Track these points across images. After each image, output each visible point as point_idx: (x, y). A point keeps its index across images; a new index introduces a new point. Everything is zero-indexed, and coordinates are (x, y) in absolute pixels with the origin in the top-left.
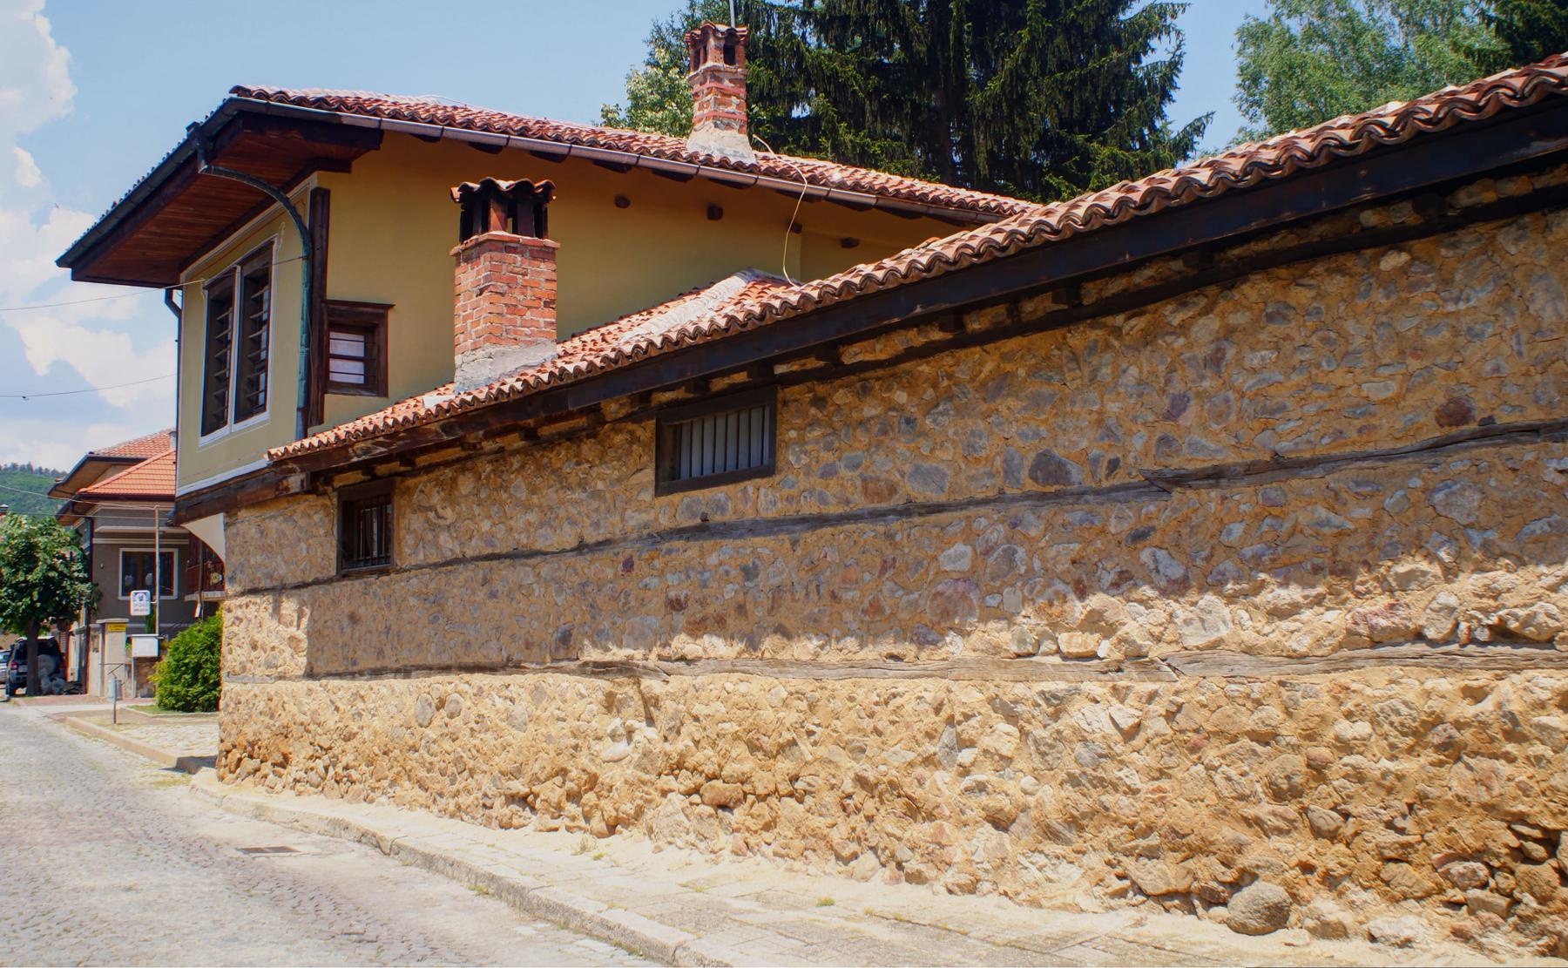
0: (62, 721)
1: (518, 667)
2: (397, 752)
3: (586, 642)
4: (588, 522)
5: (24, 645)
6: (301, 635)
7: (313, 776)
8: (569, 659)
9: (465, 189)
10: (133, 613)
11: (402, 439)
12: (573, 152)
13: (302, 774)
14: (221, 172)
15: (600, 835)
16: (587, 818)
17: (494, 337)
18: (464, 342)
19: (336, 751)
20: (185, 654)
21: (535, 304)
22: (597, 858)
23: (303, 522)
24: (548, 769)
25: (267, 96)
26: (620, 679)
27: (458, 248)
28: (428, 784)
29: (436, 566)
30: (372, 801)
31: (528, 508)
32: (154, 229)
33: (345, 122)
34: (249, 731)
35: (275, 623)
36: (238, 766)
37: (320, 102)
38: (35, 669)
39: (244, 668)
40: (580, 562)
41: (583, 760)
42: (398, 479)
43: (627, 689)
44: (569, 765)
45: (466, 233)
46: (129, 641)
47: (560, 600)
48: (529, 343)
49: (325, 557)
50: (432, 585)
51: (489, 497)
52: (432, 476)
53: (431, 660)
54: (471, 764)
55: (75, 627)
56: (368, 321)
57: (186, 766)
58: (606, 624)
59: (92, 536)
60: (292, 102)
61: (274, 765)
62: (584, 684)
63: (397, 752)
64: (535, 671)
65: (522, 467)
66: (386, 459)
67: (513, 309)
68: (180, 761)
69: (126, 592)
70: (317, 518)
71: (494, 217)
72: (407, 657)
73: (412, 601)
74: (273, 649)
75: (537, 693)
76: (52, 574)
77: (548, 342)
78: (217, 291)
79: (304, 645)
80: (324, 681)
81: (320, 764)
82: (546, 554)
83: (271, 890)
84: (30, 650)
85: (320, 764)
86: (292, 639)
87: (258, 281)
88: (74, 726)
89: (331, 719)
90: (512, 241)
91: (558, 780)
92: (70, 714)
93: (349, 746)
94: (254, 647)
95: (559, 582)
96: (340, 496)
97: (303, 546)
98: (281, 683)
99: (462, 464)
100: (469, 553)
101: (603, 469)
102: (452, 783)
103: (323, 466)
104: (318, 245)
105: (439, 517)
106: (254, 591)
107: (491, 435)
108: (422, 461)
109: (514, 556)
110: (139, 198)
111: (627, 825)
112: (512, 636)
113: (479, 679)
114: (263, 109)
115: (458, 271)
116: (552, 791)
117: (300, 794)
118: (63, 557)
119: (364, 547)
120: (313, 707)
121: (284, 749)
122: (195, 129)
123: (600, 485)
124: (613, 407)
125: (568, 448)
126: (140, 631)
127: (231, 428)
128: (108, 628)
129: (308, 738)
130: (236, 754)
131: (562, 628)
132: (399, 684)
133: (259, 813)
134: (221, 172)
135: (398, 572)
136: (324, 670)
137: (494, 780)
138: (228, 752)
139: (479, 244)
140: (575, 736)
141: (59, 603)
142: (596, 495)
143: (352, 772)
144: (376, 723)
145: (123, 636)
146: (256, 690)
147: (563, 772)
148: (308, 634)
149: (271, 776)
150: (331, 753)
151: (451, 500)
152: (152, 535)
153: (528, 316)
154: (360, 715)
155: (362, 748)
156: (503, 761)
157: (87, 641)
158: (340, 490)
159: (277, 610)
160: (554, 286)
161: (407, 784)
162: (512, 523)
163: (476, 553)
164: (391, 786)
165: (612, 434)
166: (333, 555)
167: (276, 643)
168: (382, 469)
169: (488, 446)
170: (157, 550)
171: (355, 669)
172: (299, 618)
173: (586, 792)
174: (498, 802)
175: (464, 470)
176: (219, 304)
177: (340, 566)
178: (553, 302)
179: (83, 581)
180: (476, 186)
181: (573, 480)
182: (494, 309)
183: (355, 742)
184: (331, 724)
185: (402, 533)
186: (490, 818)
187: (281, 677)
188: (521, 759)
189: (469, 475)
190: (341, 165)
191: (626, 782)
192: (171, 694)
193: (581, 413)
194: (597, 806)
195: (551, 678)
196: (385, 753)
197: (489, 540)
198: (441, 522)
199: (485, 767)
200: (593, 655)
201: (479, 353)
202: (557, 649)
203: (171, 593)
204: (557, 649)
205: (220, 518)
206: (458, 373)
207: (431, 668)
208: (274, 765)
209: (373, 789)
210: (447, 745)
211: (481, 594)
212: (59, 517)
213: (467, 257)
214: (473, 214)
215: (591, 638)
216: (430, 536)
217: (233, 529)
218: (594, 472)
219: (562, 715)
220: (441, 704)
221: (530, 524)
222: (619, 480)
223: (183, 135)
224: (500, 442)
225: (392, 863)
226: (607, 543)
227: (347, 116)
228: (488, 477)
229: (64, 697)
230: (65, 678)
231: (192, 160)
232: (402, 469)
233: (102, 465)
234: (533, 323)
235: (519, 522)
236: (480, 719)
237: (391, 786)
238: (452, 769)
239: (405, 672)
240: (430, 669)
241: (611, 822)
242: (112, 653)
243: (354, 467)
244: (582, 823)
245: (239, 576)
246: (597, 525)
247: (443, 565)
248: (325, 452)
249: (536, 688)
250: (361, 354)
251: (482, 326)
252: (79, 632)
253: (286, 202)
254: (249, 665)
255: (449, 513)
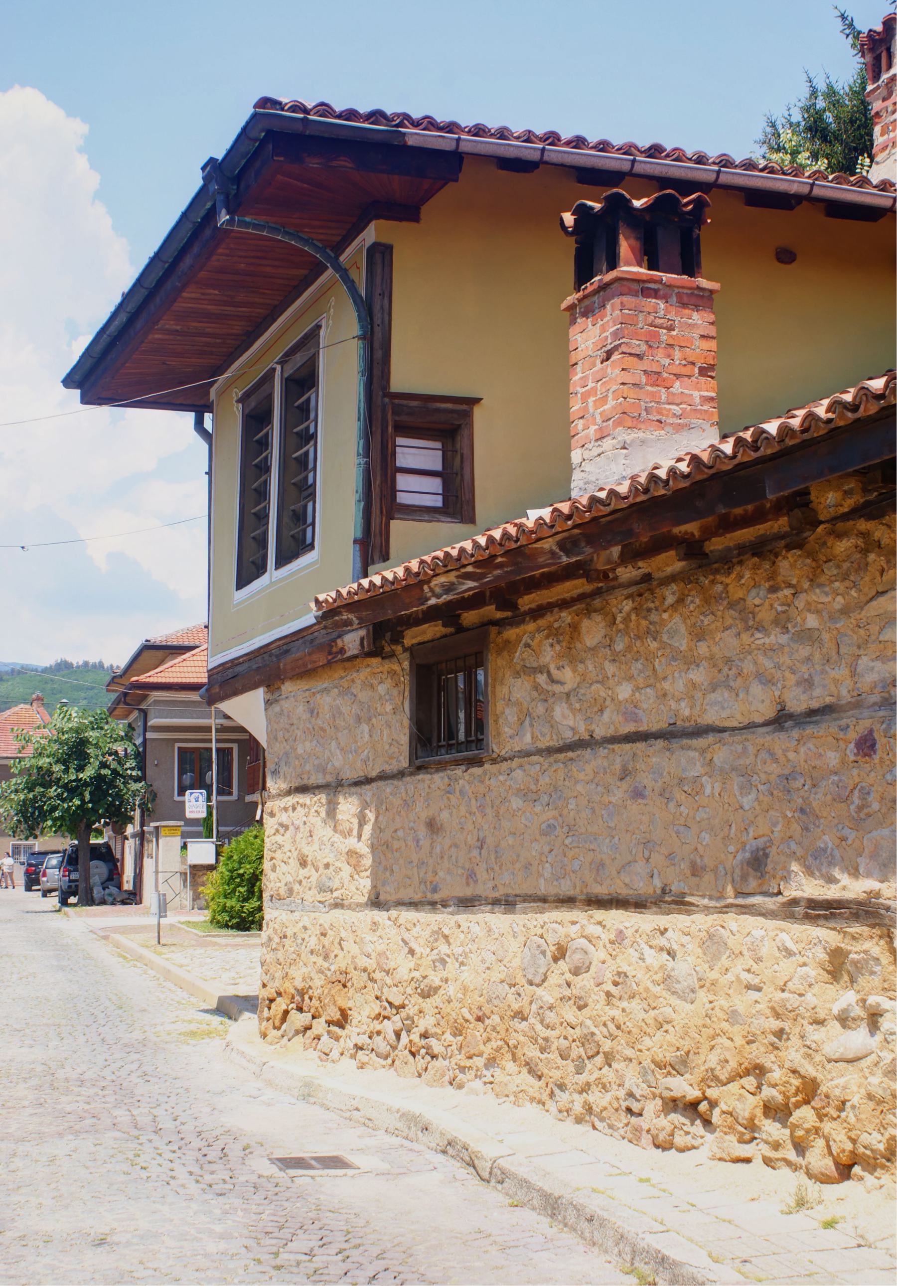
0: (106, 938)
1: (680, 904)
2: (496, 1019)
3: (795, 867)
4: (792, 679)
5: (76, 850)
6: (363, 848)
7: (380, 1043)
8: (765, 894)
9: (582, 212)
10: (189, 815)
11: (501, 566)
12: (723, 179)
13: (363, 1040)
14: (247, 225)
15: (825, 1179)
16: (800, 1147)
17: (629, 418)
18: (584, 430)
19: (411, 1010)
20: (240, 863)
21: (684, 371)
22: (830, 1224)
23: (364, 696)
24: (733, 1064)
25: (306, 111)
26: (856, 929)
27: (571, 299)
28: (542, 1068)
29: (550, 751)
30: (460, 1087)
31: (691, 661)
32: (172, 325)
33: (411, 142)
34: (298, 976)
35: (329, 831)
36: (284, 1019)
37: (376, 115)
38: (87, 877)
39: (291, 891)
40: (780, 742)
41: (793, 1054)
42: (494, 630)
43: (867, 945)
44: (767, 1061)
45: (583, 274)
46: (184, 847)
47: (747, 801)
48: (679, 428)
49: (393, 742)
50: (545, 780)
51: (629, 648)
52: (542, 622)
53: (543, 888)
54: (607, 1045)
55: (130, 829)
56: (446, 421)
57: (228, 1008)
58: (828, 840)
59: (145, 730)
60: (339, 116)
61: (329, 1023)
62: (795, 933)
63: (496, 1019)
64: (707, 910)
65: (681, 601)
66: (475, 601)
67: (655, 377)
68: (222, 1000)
69: (182, 792)
70: (382, 689)
71: (625, 247)
72: (510, 881)
73: (516, 803)
74: (327, 866)
75: (712, 944)
76: (104, 772)
77: (706, 426)
78: (253, 402)
79: (368, 861)
80: (393, 913)
81: (388, 1027)
82: (722, 730)
83: (310, 1254)
84: (81, 854)
85: (388, 1027)
86: (351, 853)
87: (303, 382)
88: (117, 945)
89: (403, 967)
90: (652, 280)
91: (750, 1082)
92: (116, 930)
93: (428, 1005)
94: (303, 863)
95: (746, 773)
96: (412, 657)
97: (365, 728)
98: (337, 912)
99: (584, 603)
100: (600, 732)
101: (818, 596)
102: (579, 1071)
103: (390, 614)
104: (377, 320)
105: (553, 681)
106: (303, 789)
107: (631, 556)
108: (527, 602)
109: (670, 734)
110: (151, 282)
111: (871, 1166)
112: (670, 856)
113: (616, 918)
114: (299, 127)
115: (574, 331)
116: (738, 1099)
117: (362, 1066)
118: (116, 753)
119: (447, 727)
120: (380, 948)
121: (342, 1003)
122: (212, 168)
123: (812, 621)
124: (831, 497)
125: (755, 568)
126: (198, 835)
127: (273, 575)
128: (162, 832)
129: (373, 990)
130: (281, 1004)
131: (752, 844)
132: (498, 920)
133: (308, 1093)
134: (247, 225)
135: (494, 761)
136: (394, 898)
137: (644, 1073)
138: (272, 1001)
139: (604, 287)
140: (777, 1016)
141: (112, 804)
142: (806, 636)
143: (433, 1042)
144: (467, 975)
145: (177, 841)
146: (306, 921)
147: (759, 1071)
148: (373, 848)
149: (325, 1038)
150: (403, 1013)
151: (571, 656)
152: (208, 729)
153: (677, 387)
154: (443, 962)
155: (446, 1009)
156: (658, 1046)
157: (142, 844)
158: (411, 650)
159: (331, 813)
160: (713, 345)
161: (511, 1066)
162: (666, 685)
163: (611, 732)
164: (487, 1066)
165: (830, 541)
166: (405, 739)
167: (330, 859)
168: (470, 617)
169: (626, 573)
170: (214, 746)
171: (437, 897)
172: (361, 825)
173: (798, 1106)
174: (652, 1107)
175: (589, 612)
176: (256, 421)
177: (414, 755)
178: (712, 367)
179: (137, 780)
180: (597, 206)
181: (765, 615)
182: (627, 378)
183: (436, 1000)
184: (403, 973)
185: (500, 705)
186: (637, 1130)
187: (337, 905)
188: (686, 1044)
189: (598, 618)
190: (407, 211)
191: (870, 1097)
192: (224, 909)
193: (779, 508)
194: (817, 1131)
195: (733, 921)
196: (479, 1019)
197: (630, 711)
198: (557, 688)
199: (629, 1052)
200: (806, 887)
201: (608, 443)
202: (744, 878)
203: (230, 793)
204: (744, 878)
205: (259, 694)
206: (576, 475)
207: (544, 900)
208: (329, 1023)
209: (463, 1069)
210: (570, 1014)
211: (619, 794)
212: (111, 711)
213: (586, 309)
214: (591, 251)
215: (802, 860)
216: (540, 709)
217: (276, 708)
218: (800, 602)
219: (756, 981)
220: (560, 953)
221: (694, 685)
222: (845, 611)
223: (197, 182)
224: (644, 567)
225: (493, 1196)
226: (827, 710)
227: (414, 136)
228: (626, 620)
229: (120, 907)
230: (119, 886)
231: (212, 214)
232: (499, 615)
233: (160, 654)
234: (683, 399)
235: (677, 684)
236: (621, 978)
237: (487, 1066)
238: (577, 1051)
239: (507, 903)
240: (543, 901)
241: (844, 1159)
242: (167, 859)
243: (432, 615)
244: (791, 1155)
245: (284, 769)
246: (808, 683)
247: (560, 750)
248: (390, 595)
249: (711, 936)
250: (438, 467)
251: (611, 403)
252: (134, 836)
253: (338, 268)
254: (296, 887)
255: (568, 676)
